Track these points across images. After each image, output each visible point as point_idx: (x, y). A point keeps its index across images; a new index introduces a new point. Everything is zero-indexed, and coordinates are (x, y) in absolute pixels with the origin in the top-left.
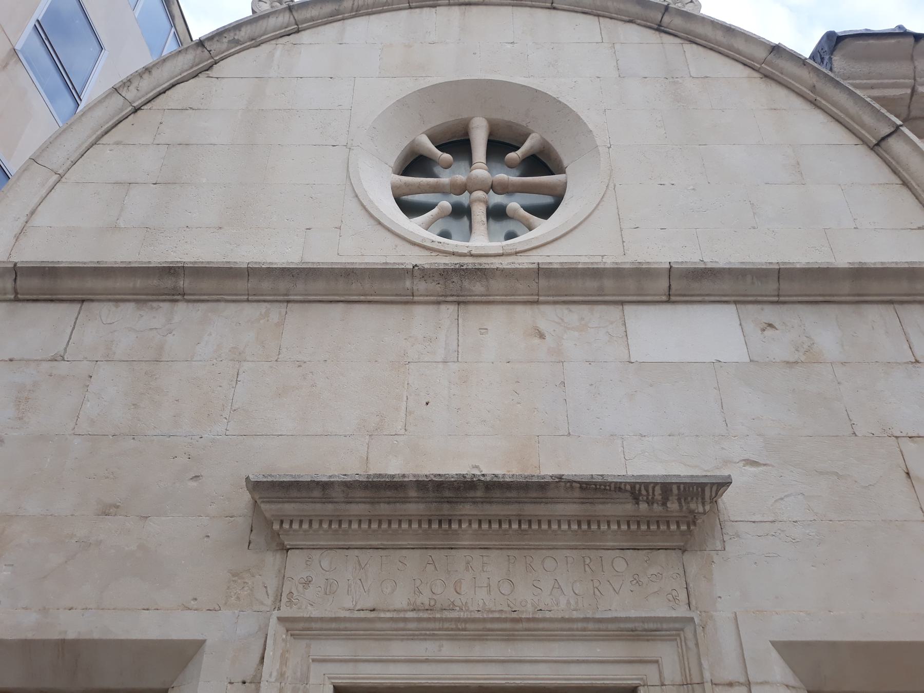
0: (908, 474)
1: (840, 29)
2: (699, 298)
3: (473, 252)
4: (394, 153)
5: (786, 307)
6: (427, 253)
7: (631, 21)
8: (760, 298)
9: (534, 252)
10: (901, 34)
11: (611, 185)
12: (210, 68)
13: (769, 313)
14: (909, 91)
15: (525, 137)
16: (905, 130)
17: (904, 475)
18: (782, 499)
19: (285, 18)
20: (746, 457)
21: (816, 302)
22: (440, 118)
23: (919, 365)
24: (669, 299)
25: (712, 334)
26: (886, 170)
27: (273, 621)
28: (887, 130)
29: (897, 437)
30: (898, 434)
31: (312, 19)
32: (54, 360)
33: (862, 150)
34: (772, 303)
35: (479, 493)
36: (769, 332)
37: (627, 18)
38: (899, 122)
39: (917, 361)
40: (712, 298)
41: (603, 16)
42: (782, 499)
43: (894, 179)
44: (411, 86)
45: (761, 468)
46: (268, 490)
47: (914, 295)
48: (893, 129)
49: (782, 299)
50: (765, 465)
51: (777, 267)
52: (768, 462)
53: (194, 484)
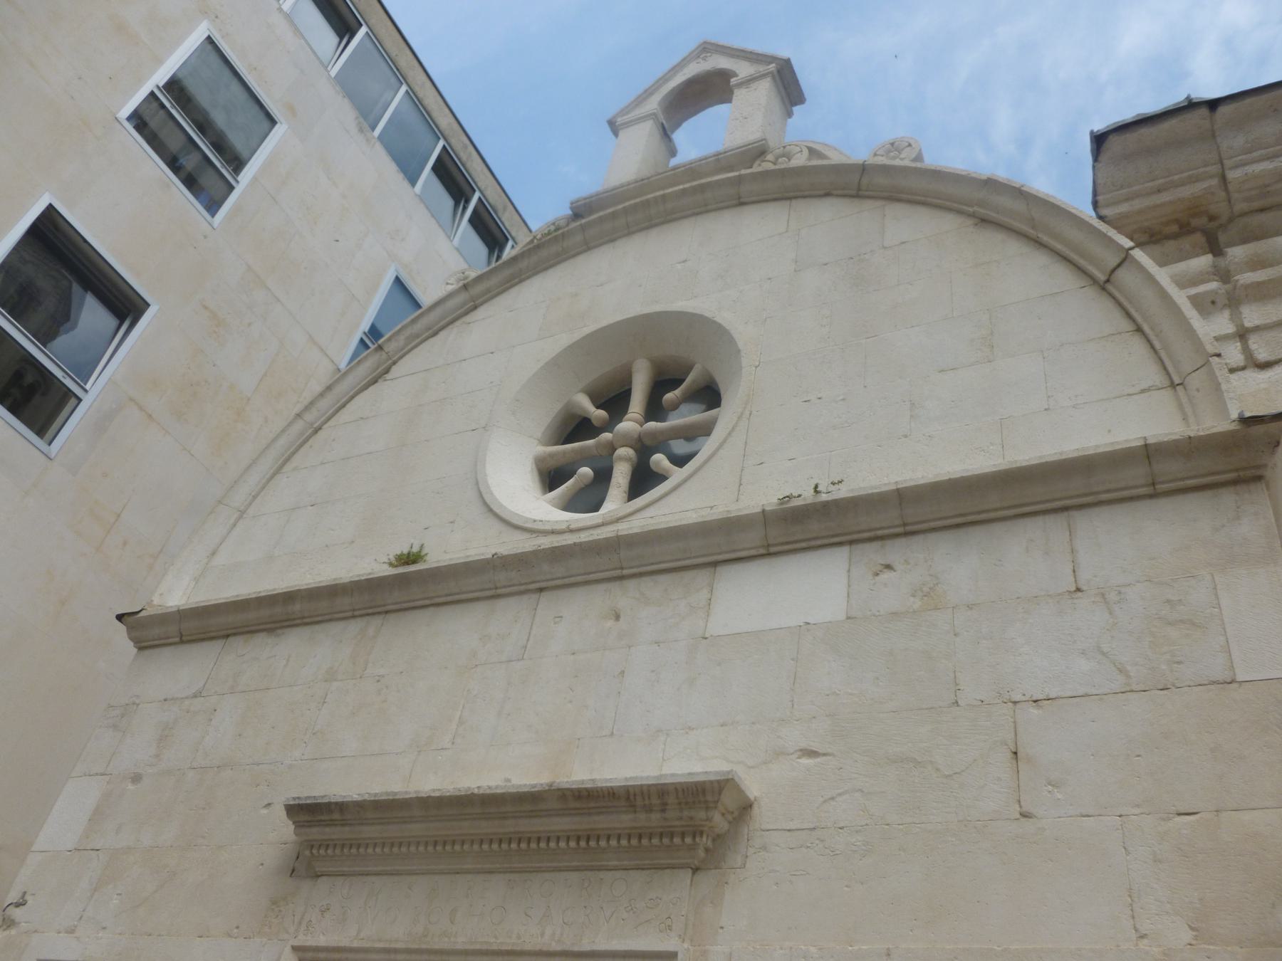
0: (1015, 753)
1: (1100, 126)
2: (804, 545)
3: (572, 527)
4: (544, 415)
5: (919, 538)
6: (527, 535)
7: (827, 195)
8: (880, 533)
9: (639, 516)
10: (1191, 105)
11: (747, 413)
12: (387, 371)
13: (873, 554)
14: (1215, 182)
15: (689, 368)
16: (1138, 254)
17: (1010, 755)
18: (833, 798)
19: (463, 297)
20: (803, 745)
21: (958, 526)
22: (598, 370)
23: (1079, 594)
24: (768, 552)
25: (813, 590)
26: (1117, 315)
27: (288, 949)
28: (1113, 261)
29: (1015, 703)
30: (1018, 697)
31: (488, 291)
32: (195, 696)
33: (1091, 292)
34: (762, 556)
35: (336, 816)
36: (886, 576)
37: (822, 192)
38: (1127, 243)
39: (1078, 590)
40: (819, 542)
41: (796, 198)
42: (833, 798)
43: (1125, 325)
44: (565, 340)
45: (818, 760)
46: (307, 813)
47: (850, 533)
48: (1123, 256)
49: (909, 528)
50: (824, 755)
51: (894, 487)
52: (829, 751)
53: (265, 811)
